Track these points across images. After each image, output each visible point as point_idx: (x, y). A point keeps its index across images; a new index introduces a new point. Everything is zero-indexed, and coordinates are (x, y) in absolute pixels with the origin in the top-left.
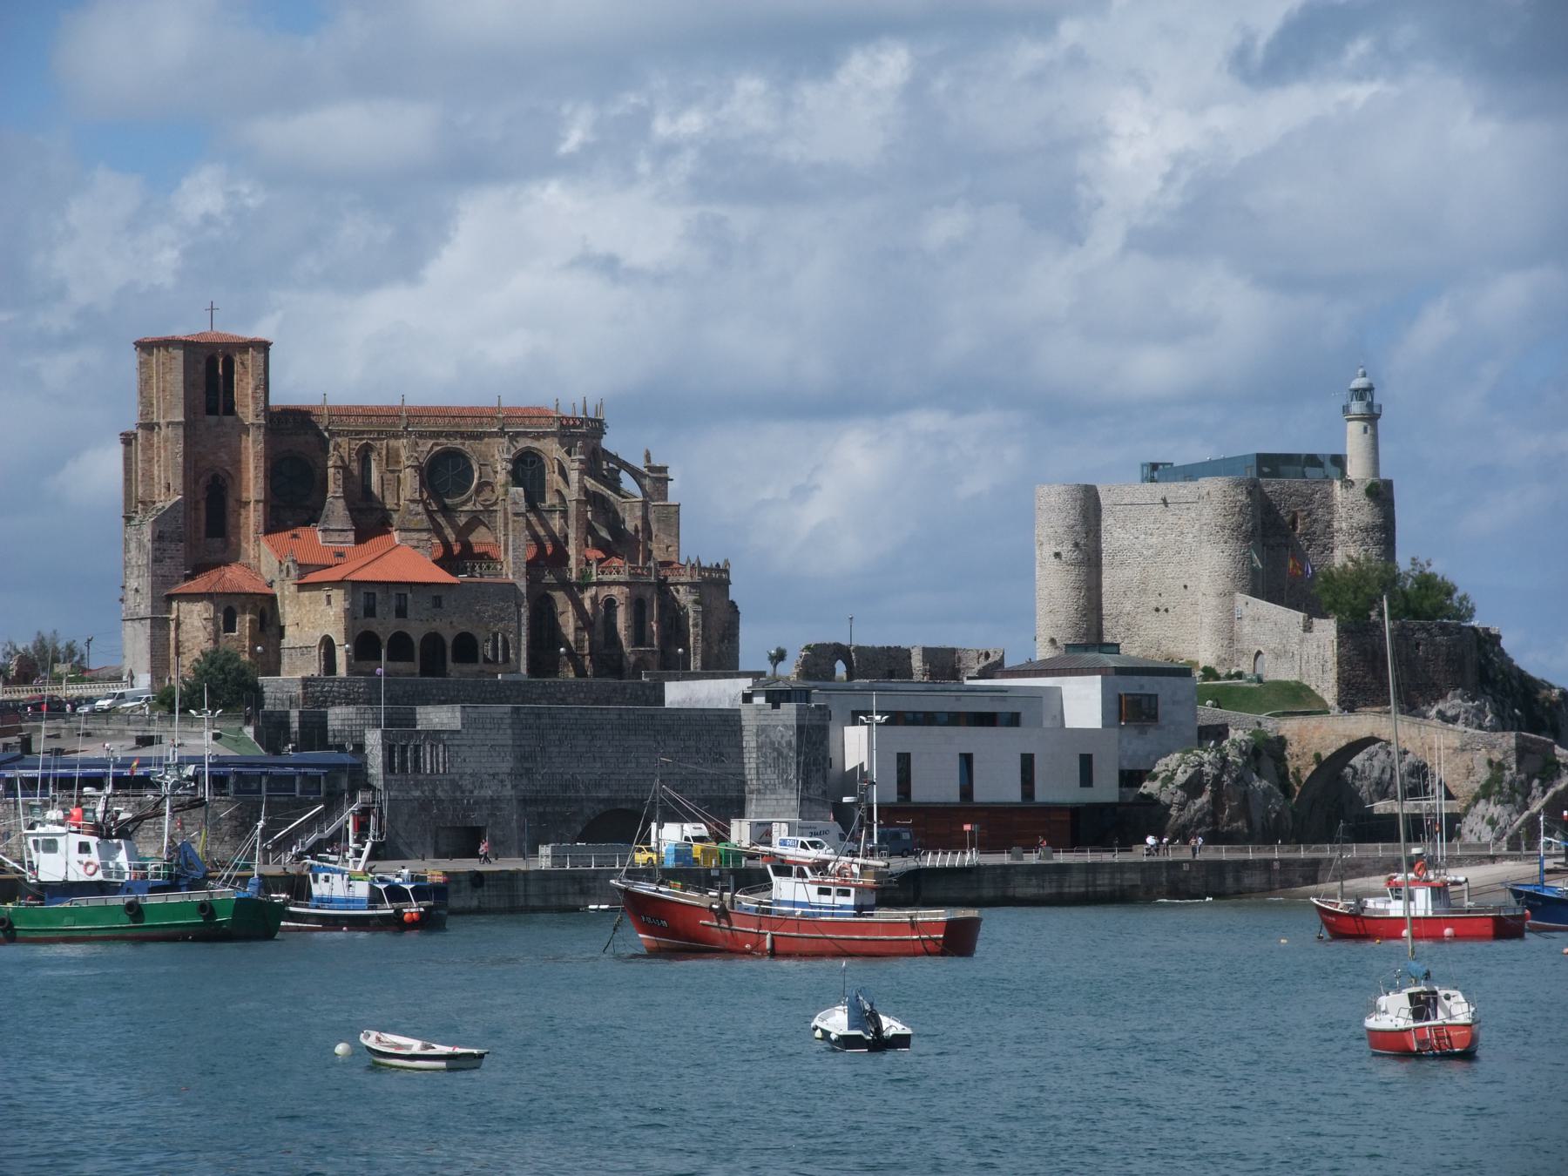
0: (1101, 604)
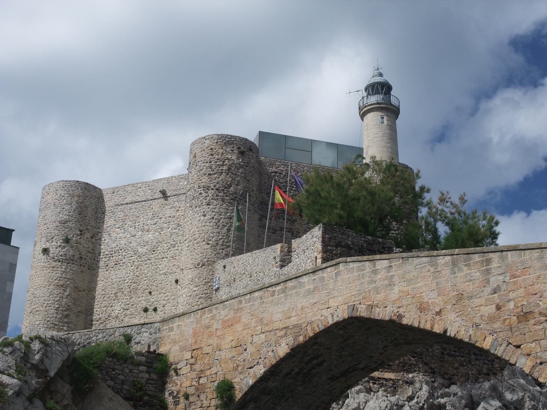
0: (92, 309)
